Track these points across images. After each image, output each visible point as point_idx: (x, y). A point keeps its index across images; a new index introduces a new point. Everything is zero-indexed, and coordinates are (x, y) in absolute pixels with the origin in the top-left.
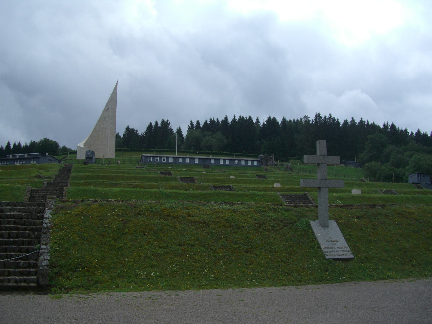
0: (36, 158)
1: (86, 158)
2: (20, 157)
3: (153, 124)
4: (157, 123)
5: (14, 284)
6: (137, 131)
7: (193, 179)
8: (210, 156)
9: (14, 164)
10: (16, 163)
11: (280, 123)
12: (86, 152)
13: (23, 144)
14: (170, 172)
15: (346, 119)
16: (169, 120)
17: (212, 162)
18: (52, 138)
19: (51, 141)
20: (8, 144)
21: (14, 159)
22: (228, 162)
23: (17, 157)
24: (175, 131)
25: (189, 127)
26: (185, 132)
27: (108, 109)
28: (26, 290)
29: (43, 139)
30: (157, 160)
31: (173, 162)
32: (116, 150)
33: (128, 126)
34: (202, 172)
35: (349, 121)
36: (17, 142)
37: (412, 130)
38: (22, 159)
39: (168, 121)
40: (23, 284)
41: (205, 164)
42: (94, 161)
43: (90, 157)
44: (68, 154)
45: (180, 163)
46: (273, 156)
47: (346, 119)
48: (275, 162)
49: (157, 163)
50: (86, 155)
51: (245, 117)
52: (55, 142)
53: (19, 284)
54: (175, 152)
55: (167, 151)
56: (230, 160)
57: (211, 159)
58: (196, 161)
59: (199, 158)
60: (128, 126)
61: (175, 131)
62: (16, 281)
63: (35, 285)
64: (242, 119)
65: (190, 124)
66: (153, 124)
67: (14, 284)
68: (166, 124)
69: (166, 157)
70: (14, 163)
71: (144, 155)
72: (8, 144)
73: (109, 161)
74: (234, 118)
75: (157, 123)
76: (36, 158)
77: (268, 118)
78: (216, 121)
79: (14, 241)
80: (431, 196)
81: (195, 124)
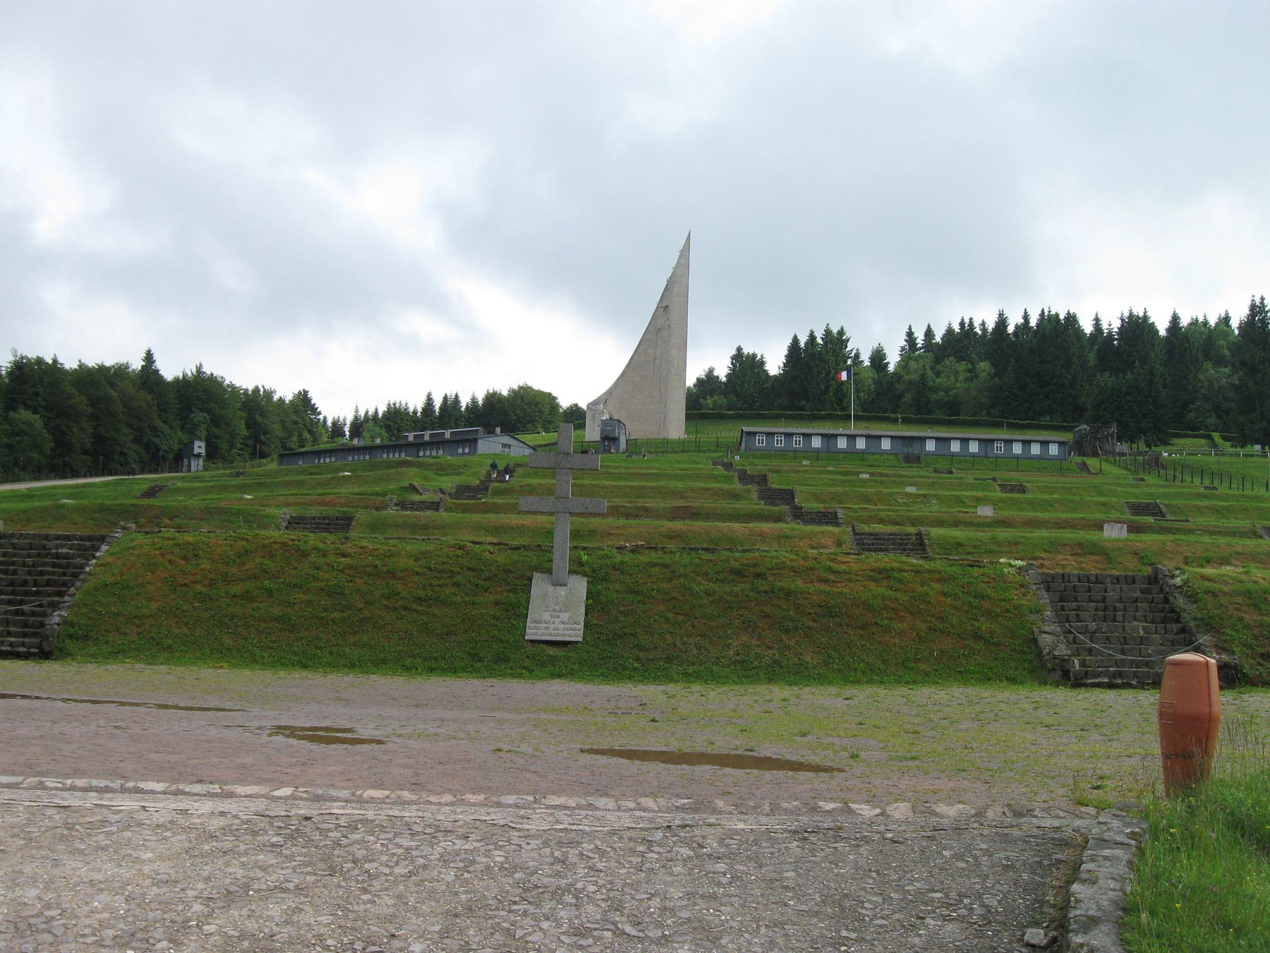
0: (469, 440)
1: (601, 438)
2: (457, 438)
3: (803, 341)
4: (812, 337)
5: (9, 648)
6: (762, 363)
7: (792, 493)
8: (926, 431)
9: (418, 457)
10: (421, 453)
11: (1162, 333)
12: (602, 424)
13: (465, 401)
14: (765, 476)
15: (15, 352)
16: (846, 329)
17: (930, 446)
18: (540, 384)
19: (539, 392)
20: (429, 402)
21: (419, 445)
22: (974, 447)
23: (427, 438)
24: (866, 359)
25: (903, 349)
26: (893, 359)
27: (667, 306)
28: (26, 656)
29: (504, 388)
30: (779, 443)
31: (1040, 456)
32: (689, 417)
33: (739, 349)
34: (858, 473)
35: (1201, 319)
36: (451, 394)
37: (70, 363)
38: (438, 443)
39: (841, 332)
40: (21, 649)
41: (910, 454)
42: (623, 446)
43: (611, 436)
44: (348, 423)
45: (841, 451)
46: (1114, 429)
47: (15, 352)
48: (1122, 447)
49: (780, 450)
50: (602, 431)
51: (977, 324)
52: (550, 394)
53: (16, 649)
54: (848, 417)
55: (751, 417)
56: (980, 440)
57: (926, 438)
58: (886, 445)
59: (892, 437)
60: (739, 349)
61: (866, 359)
62: (11, 644)
63: (37, 650)
64: (1049, 321)
65: (906, 341)
66: (803, 341)
67: (9, 648)
68: (836, 342)
69: (804, 435)
70: (418, 454)
71: (745, 429)
72: (429, 402)
73: (664, 447)
74: (1022, 321)
75: (812, 337)
76: (469, 440)
77: (1122, 320)
78: (980, 332)
79: (48, 581)
80: (1269, 522)
81: (920, 340)
